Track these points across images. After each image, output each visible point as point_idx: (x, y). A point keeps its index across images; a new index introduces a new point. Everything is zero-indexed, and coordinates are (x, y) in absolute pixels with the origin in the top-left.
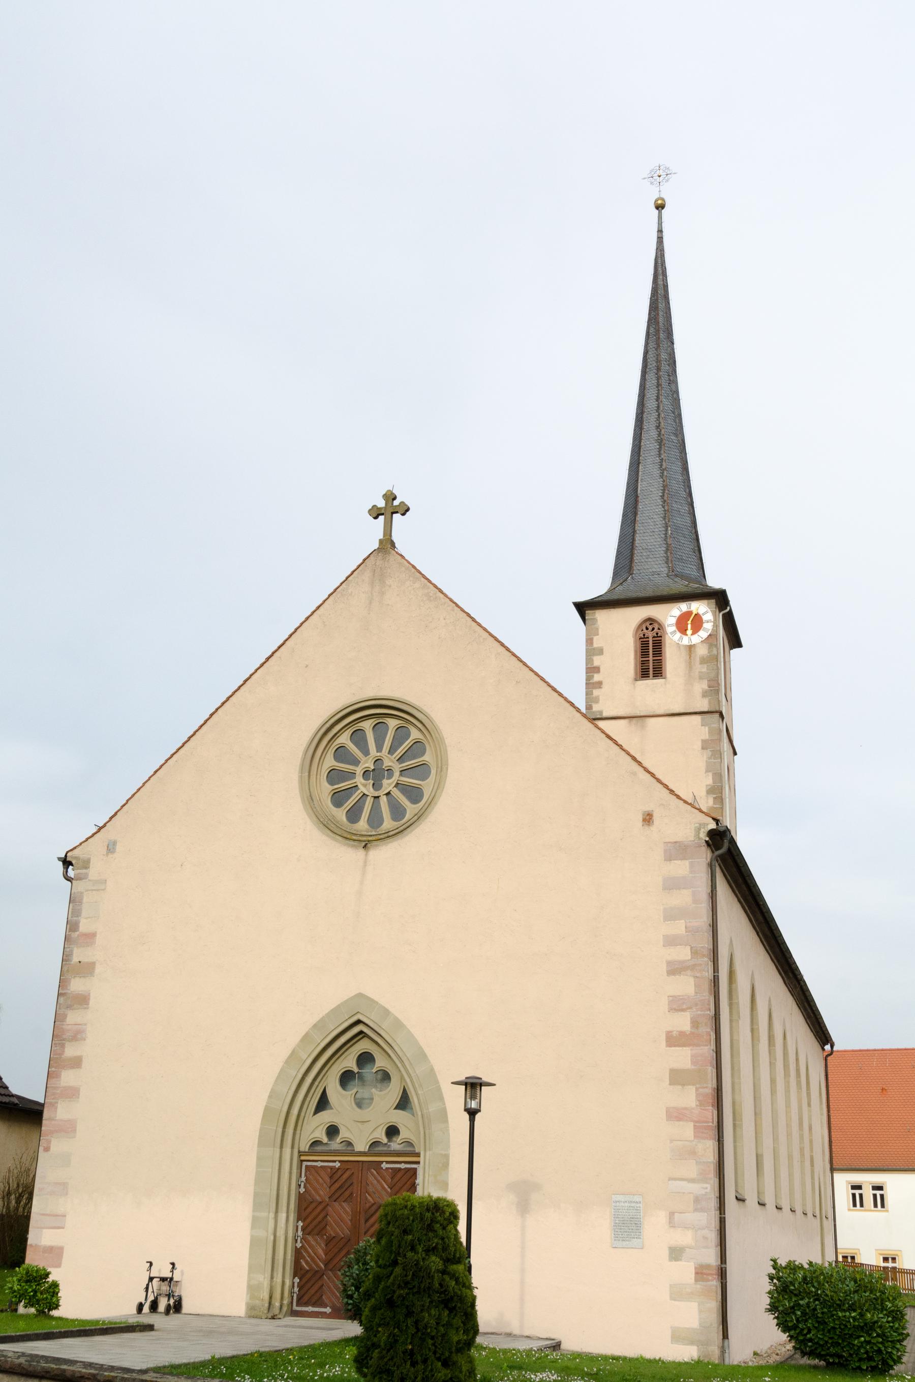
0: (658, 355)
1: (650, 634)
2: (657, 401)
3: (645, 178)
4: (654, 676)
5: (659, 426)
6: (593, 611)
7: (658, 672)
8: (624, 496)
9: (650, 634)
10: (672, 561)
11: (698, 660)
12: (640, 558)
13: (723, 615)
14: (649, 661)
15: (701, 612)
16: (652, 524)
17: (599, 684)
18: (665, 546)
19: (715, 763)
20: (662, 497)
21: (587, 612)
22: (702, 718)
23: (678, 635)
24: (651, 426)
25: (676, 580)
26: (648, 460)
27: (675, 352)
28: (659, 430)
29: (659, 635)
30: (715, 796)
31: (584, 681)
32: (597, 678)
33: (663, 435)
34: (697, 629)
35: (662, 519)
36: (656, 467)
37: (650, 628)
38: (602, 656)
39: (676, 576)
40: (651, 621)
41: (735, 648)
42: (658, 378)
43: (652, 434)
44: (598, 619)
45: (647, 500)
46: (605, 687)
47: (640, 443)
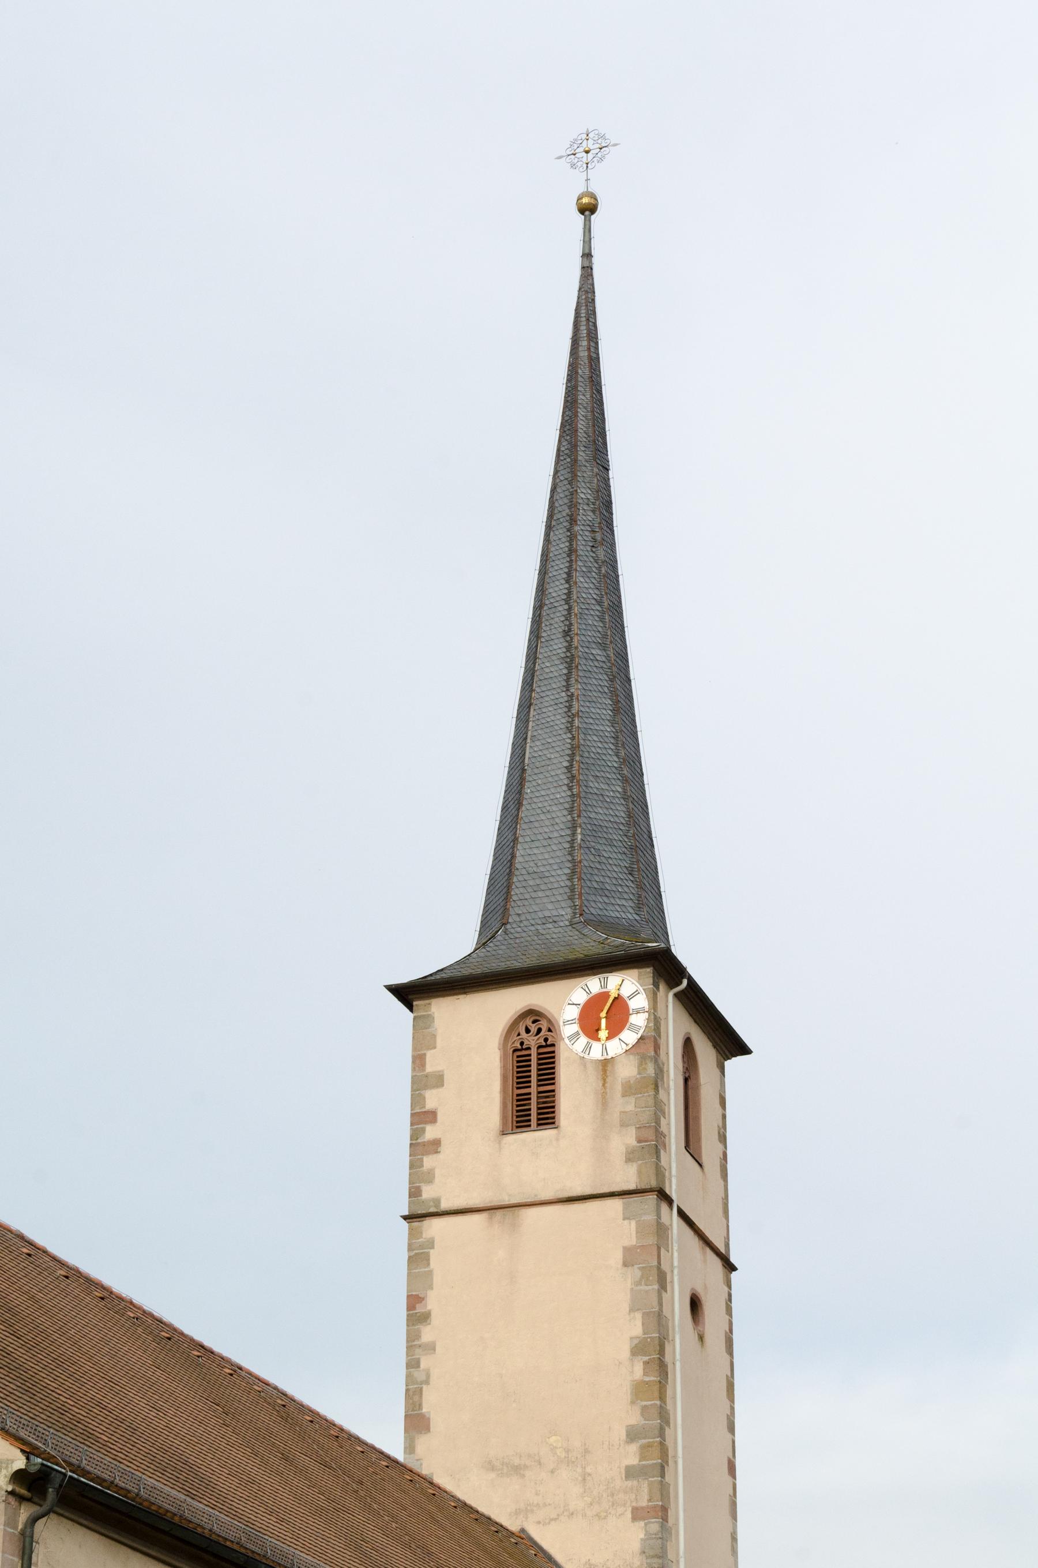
0: (573, 493)
1: (532, 1041)
2: (567, 582)
3: (560, 157)
4: (539, 1125)
5: (570, 630)
6: (427, 1002)
7: (547, 1117)
8: (507, 769)
9: (532, 1041)
10: (581, 894)
11: (619, 1088)
12: (522, 890)
13: (676, 995)
14: (530, 1094)
15: (625, 992)
16: (547, 823)
17: (435, 1146)
18: (569, 865)
19: (647, 1292)
20: (569, 769)
21: (415, 1003)
22: (624, 1203)
23: (583, 1040)
24: (554, 631)
25: (585, 931)
26: (547, 699)
27: (612, 484)
28: (568, 638)
29: (549, 1043)
30: (646, 1358)
31: (407, 1142)
32: (431, 1132)
33: (576, 648)
34: (617, 1026)
35: (565, 813)
36: (560, 711)
37: (533, 1028)
38: (440, 1090)
39: (587, 922)
40: (533, 1015)
41: (735, 1056)
42: (572, 538)
43: (555, 647)
44: (436, 1015)
45: (541, 776)
46: (446, 1149)
47: (534, 666)
